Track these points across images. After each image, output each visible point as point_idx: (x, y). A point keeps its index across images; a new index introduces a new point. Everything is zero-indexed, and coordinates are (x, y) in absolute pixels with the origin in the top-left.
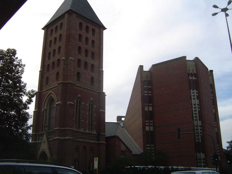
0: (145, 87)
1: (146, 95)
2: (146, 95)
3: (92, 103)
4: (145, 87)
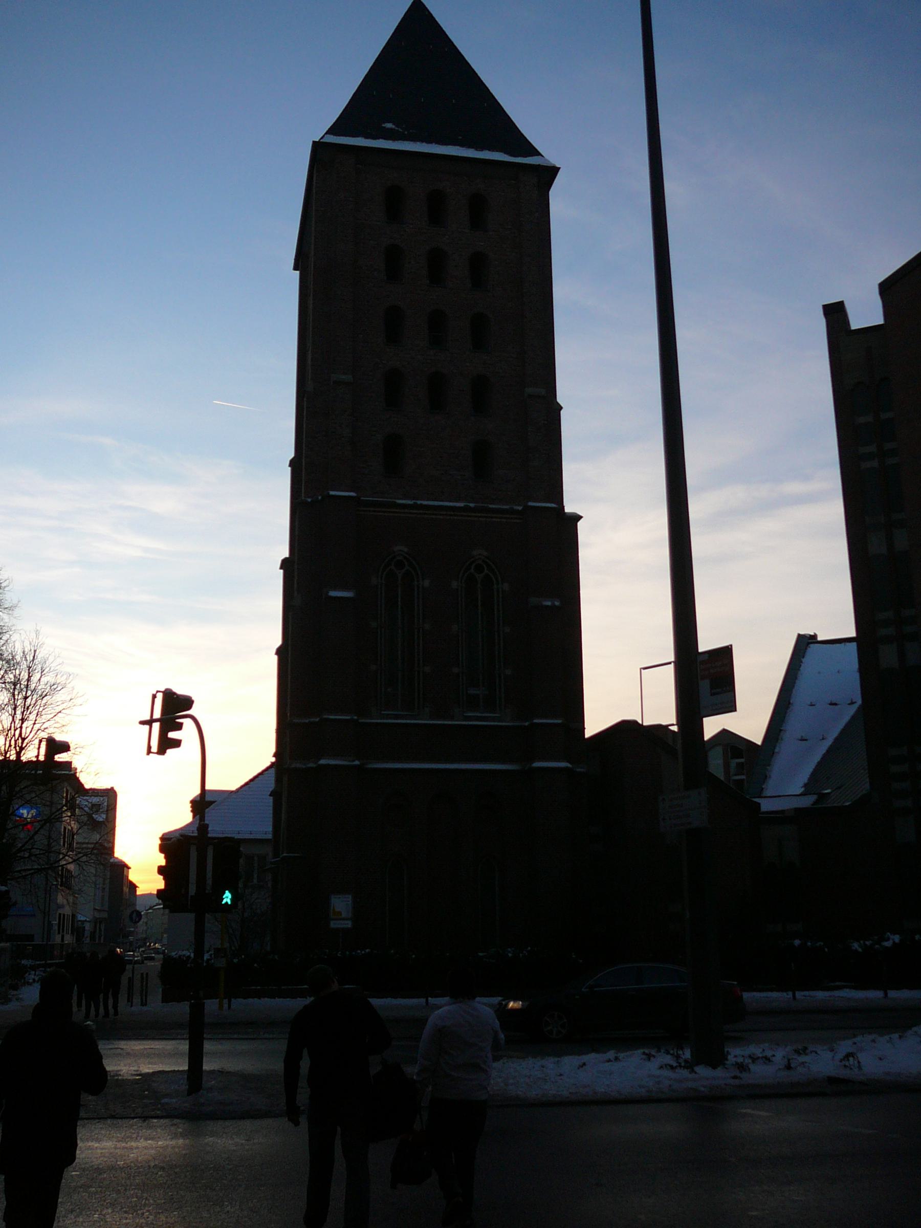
0: (862, 420)
1: (875, 464)
2: (875, 464)
3: (486, 571)
4: (862, 420)
